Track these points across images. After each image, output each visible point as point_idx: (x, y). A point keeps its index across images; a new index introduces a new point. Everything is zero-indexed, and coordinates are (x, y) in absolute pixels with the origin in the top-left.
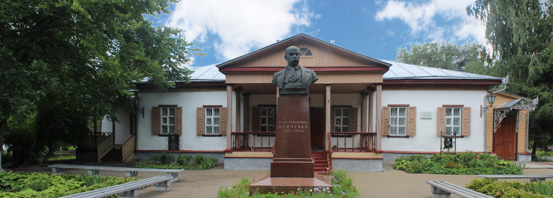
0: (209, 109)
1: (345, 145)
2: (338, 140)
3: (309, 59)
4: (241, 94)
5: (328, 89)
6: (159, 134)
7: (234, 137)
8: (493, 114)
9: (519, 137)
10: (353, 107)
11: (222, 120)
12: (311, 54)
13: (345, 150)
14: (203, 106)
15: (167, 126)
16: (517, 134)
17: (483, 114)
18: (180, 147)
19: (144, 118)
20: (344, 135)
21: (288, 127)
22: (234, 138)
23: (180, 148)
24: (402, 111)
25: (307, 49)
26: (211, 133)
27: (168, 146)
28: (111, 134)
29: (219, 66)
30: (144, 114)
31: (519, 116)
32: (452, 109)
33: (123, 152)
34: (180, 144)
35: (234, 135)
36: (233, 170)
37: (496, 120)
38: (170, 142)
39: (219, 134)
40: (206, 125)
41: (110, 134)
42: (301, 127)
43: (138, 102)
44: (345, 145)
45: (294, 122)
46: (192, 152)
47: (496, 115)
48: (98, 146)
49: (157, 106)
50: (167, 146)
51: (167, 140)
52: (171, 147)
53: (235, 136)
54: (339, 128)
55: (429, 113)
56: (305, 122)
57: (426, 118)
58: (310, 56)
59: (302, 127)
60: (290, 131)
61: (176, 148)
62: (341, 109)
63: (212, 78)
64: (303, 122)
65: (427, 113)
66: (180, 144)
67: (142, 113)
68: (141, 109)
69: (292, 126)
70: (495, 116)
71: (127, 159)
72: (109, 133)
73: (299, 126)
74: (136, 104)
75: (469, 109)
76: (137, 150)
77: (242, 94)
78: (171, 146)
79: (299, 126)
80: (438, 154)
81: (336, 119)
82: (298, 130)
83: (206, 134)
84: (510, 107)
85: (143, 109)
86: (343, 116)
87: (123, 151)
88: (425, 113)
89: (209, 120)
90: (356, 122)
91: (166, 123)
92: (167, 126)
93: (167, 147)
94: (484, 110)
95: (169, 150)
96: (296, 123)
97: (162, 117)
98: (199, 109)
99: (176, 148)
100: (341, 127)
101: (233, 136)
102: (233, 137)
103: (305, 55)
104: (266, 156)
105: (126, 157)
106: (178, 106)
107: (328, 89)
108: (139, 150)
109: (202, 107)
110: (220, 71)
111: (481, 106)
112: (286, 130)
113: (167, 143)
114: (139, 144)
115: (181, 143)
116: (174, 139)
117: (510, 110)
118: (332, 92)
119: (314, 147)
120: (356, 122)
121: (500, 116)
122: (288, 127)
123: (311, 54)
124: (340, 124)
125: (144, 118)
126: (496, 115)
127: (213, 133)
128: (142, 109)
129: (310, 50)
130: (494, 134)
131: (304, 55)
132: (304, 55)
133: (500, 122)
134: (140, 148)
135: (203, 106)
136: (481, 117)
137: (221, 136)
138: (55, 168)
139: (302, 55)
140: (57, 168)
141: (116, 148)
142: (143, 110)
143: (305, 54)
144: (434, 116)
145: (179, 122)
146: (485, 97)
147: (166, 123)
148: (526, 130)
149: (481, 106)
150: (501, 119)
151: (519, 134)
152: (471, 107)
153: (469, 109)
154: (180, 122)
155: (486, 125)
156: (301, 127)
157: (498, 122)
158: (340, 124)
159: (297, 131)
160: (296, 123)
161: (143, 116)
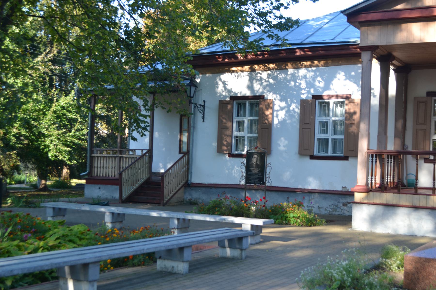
4: (392, 67)
6: (312, 154)
7: (392, 162)
15: (328, 139)
18: (266, 178)
19: (203, 121)
22: (392, 164)
23: (267, 179)
24: (324, 106)
26: (327, 152)
27: (245, 175)
28: (146, 151)
29: (347, 12)
30: (204, 114)
33: (165, 186)
34: (266, 172)
35: (391, 159)
38: (248, 167)
39: (342, 155)
41: (145, 152)
43: (195, 92)
48: (166, 175)
50: (242, 176)
51: (243, 163)
52: (250, 177)
53: (392, 160)
61: (259, 181)
63: (333, 39)
66: (268, 172)
67: (201, 113)
68: (200, 105)
71: (171, 200)
72: (142, 150)
74: (192, 95)
76: (189, 182)
77: (394, 70)
78: (250, 175)
83: (316, 153)
85: (203, 104)
87: (166, 183)
91: (327, 133)
93: (244, 178)
95: (246, 182)
97: (318, 119)
99: (259, 181)
101: (390, 160)
102: (390, 162)
105: (171, 195)
110: (348, 21)
113: (244, 170)
114: (193, 171)
115: (268, 170)
116: (257, 161)
125: (203, 121)
127: (330, 153)
134: (195, 180)
137: (346, 158)
138: (50, 207)
140: (54, 208)
141: (153, 178)
142: (204, 106)
145: (267, 130)
147: (327, 133)
154: (268, 128)
161: (203, 117)
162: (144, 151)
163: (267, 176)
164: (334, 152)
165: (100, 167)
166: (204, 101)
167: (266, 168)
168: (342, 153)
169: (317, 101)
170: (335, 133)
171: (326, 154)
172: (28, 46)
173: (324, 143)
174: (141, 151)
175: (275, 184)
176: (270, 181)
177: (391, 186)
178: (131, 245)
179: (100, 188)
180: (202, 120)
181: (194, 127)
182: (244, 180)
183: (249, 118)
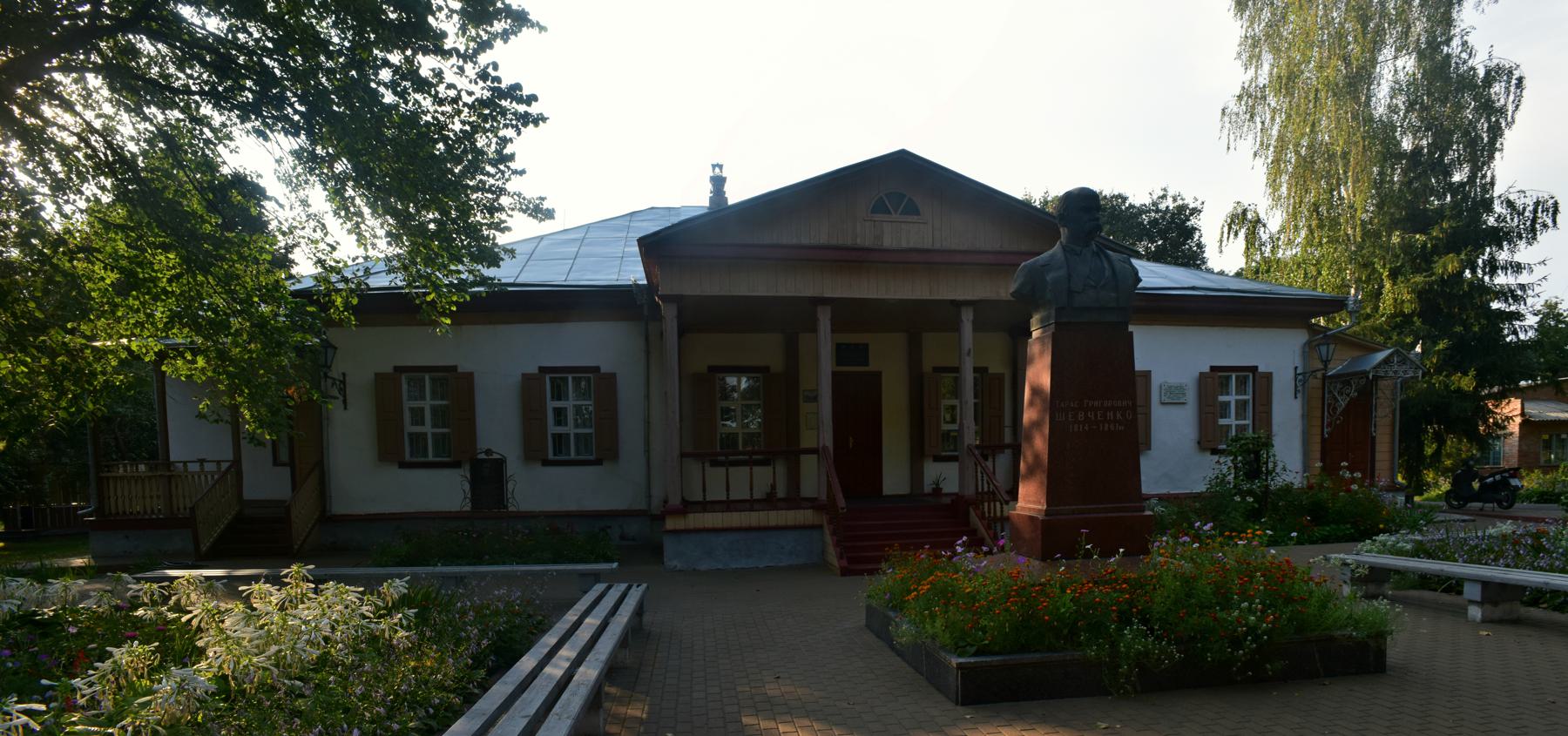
0: (557, 377)
1: (728, 490)
2: (774, 473)
5: (967, 316)
8: (1321, 391)
9: (1378, 448)
10: (991, 371)
12: (917, 213)
13: (729, 505)
16: (1373, 439)
17: (1300, 388)
19: (345, 408)
20: (747, 457)
21: (1081, 416)
26: (570, 455)
28: (227, 464)
31: (1379, 392)
32: (1231, 376)
36: (694, 570)
37: (1329, 405)
38: (475, 482)
40: (553, 429)
41: (224, 466)
42: (1115, 415)
44: (728, 490)
45: (1096, 403)
47: (1330, 392)
49: (389, 369)
50: (465, 498)
54: (952, 434)
55: (1181, 387)
56: (1125, 403)
57: (1174, 398)
59: (1118, 416)
60: (1086, 428)
64: (1119, 403)
66: (510, 490)
69: (1091, 415)
70: (1326, 396)
72: (218, 462)
73: (1110, 415)
75: (1268, 377)
79: (1110, 415)
80: (1154, 501)
82: (1107, 425)
83: (551, 456)
84: (1369, 372)
88: (1170, 387)
89: (560, 415)
93: (468, 500)
94: (1302, 380)
95: (473, 508)
96: (1102, 404)
98: (379, 377)
106: (460, 370)
107: (967, 316)
108: (335, 516)
111: (1296, 368)
112: (1076, 426)
113: (467, 487)
115: (510, 486)
117: (1368, 378)
118: (978, 327)
121: (1341, 393)
122: (1081, 416)
123: (917, 213)
125: (345, 408)
126: (1330, 392)
128: (341, 381)
130: (1323, 440)
131: (896, 211)
133: (1339, 410)
136: (1296, 397)
137: (598, 462)
139: (890, 213)
142: (343, 382)
143: (900, 210)
144: (1191, 396)
146: (1305, 344)
148: (1393, 430)
149: (1296, 368)
150: (1343, 403)
151: (1378, 440)
152: (1271, 374)
153: (1268, 377)
155: (1306, 416)
156: (1115, 415)
157: (1335, 409)
159: (1106, 429)
160: (1102, 404)
162: (205, 464)
163: (509, 496)
164: (578, 453)
165: (184, 497)
166: (344, 374)
167: (507, 483)
168: (449, 456)
169: (404, 378)
170: (577, 426)
171: (566, 458)
172: (431, 221)
173: (560, 440)
174: (198, 464)
175: (525, 507)
176: (515, 503)
177: (983, 489)
178: (584, 634)
179: (127, 537)
180: (343, 406)
181: (328, 419)
182: (470, 505)
183: (432, 402)
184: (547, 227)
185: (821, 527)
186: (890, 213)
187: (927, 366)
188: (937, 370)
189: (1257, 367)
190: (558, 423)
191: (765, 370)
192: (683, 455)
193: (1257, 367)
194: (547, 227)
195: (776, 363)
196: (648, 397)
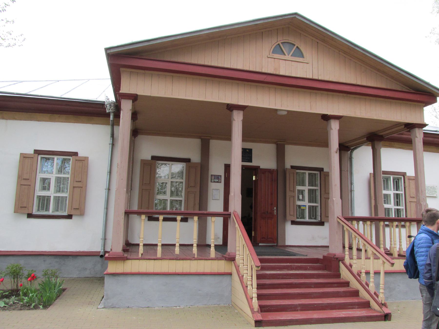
3: (298, 63)
11: (75, 183)
12: (303, 56)
14: (35, 150)
25: (294, 45)
40: (39, 193)
46: (8, 253)
58: (301, 59)
62: (305, 173)
65: (431, 187)
81: (297, 190)
83: (35, 212)
86: (309, 186)
90: (294, 196)
91: (49, 189)
92: (49, 197)
98: (24, 157)
100: (305, 206)
103: (291, 56)
104: (208, 270)
109: (32, 152)
119: (260, 244)
120: (294, 196)
123: (303, 56)
124: (303, 200)
129: (298, 46)
131: (288, 55)
132: (288, 55)
135: (35, 150)
137: (69, 217)
139: (285, 55)
158: (303, 200)
169: (40, 157)
184: (156, 194)
185: (230, 274)
186: (285, 55)
187: (288, 166)
188: (292, 167)
189: (405, 173)
190: (44, 189)
191: (187, 161)
192: (128, 213)
193: (405, 173)
194: (156, 194)
195: (196, 158)
196: (110, 172)
